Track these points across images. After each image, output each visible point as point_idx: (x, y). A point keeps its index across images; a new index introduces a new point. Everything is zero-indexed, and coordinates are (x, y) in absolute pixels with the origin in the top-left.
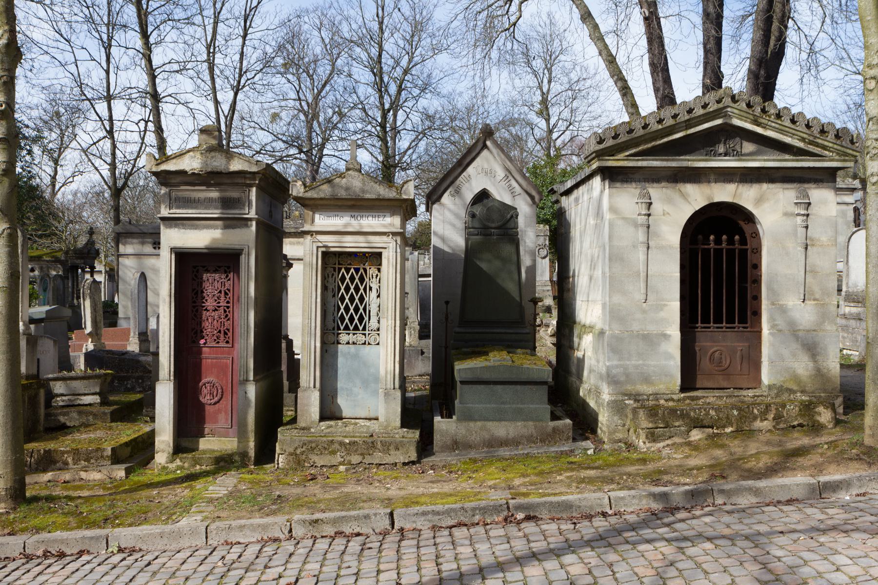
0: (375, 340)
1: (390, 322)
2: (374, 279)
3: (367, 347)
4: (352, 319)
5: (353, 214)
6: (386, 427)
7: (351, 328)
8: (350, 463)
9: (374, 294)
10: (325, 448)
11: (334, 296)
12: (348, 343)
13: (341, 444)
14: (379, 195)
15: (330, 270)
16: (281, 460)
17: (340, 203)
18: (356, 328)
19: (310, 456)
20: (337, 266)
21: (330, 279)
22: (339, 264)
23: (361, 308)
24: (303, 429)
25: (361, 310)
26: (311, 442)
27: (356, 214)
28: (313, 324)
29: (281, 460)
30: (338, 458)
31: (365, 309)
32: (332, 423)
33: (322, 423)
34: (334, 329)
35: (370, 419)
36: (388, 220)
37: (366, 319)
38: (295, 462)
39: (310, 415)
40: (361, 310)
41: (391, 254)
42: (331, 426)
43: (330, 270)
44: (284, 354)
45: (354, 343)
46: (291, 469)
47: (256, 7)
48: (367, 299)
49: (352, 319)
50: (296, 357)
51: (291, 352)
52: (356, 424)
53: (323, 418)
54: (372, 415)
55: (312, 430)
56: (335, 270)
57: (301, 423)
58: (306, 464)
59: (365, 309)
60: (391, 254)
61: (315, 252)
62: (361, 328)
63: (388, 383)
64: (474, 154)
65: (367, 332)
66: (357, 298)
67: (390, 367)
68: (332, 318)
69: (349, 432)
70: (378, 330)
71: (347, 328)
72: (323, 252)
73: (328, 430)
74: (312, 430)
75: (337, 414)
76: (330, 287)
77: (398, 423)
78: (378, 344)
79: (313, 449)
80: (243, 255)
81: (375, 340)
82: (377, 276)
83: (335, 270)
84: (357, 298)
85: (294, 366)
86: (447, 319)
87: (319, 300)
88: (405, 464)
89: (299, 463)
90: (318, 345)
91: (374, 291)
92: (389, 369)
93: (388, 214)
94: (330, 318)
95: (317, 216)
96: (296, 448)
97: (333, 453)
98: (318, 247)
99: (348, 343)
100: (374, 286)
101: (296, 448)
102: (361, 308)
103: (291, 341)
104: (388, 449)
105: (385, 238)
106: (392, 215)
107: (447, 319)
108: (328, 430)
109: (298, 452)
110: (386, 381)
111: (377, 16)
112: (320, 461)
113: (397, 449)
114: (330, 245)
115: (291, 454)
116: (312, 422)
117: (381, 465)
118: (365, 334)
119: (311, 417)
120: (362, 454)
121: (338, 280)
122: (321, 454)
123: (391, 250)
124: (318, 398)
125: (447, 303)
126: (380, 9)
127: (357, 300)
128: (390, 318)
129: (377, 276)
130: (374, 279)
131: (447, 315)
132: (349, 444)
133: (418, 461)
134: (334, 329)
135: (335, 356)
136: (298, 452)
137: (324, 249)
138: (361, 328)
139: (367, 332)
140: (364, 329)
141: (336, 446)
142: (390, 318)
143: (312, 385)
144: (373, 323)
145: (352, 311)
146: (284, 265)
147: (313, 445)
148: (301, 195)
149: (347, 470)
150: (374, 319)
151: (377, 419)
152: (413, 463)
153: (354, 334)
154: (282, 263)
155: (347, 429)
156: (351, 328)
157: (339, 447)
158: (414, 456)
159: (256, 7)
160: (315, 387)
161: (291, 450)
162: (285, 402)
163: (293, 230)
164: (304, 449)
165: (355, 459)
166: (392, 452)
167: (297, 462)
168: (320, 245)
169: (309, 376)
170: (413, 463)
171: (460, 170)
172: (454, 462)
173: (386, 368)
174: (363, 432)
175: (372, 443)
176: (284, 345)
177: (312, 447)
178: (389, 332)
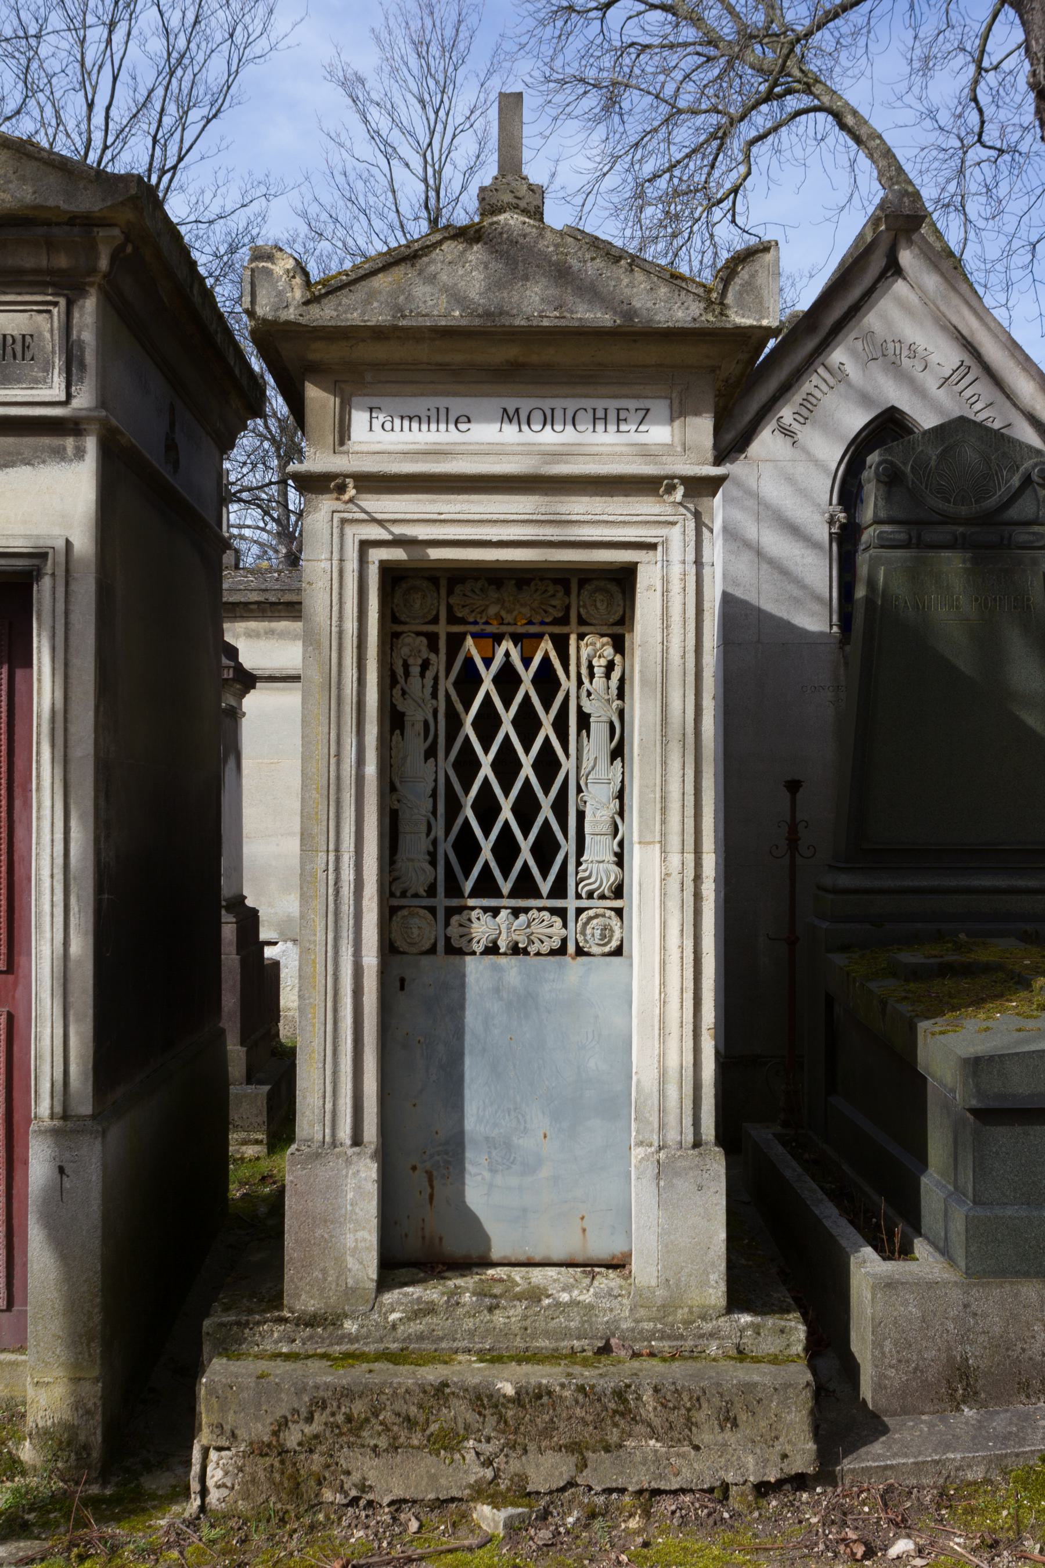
0: (606, 933)
1: (675, 859)
2: (599, 681)
3: (573, 967)
4: (506, 850)
5: (511, 404)
6: (666, 1309)
7: (506, 887)
8: (523, 1494)
9: (597, 744)
10: (410, 1422)
11: (431, 753)
12: (492, 950)
13: (483, 1400)
14: (630, 314)
15: (413, 646)
16: (217, 1471)
17: (458, 358)
18: (526, 887)
19: (347, 1458)
20: (442, 629)
21: (415, 681)
22: (452, 619)
23: (546, 802)
24: (311, 1321)
25: (546, 812)
26: (347, 1393)
27: (525, 405)
28: (348, 875)
29: (215, 1475)
30: (469, 1469)
31: (560, 807)
32: (431, 1293)
33: (389, 1297)
34: (432, 891)
35: (589, 1266)
36: (659, 433)
37: (568, 847)
38: (276, 1486)
39: (339, 1261)
40: (546, 812)
41: (676, 570)
42: (430, 1309)
43: (413, 646)
44: (230, 958)
45: (516, 950)
46: (262, 1516)
47: (174, 168)
48: (568, 765)
49: (506, 850)
50: (269, 952)
51: (250, 941)
52: (535, 1295)
53: (398, 1264)
54: (601, 1247)
55: (350, 1326)
56: (433, 647)
57: (303, 1295)
58: (328, 1495)
59: (560, 807)
60: (676, 570)
61: (352, 565)
62: (545, 887)
63: (672, 1119)
64: (856, 293)
65: (571, 904)
66: (527, 761)
67: (677, 1054)
68: (424, 844)
69: (506, 1333)
70: (618, 892)
71: (486, 886)
72: (387, 570)
73: (416, 1327)
74: (350, 1326)
75: (455, 1246)
76: (416, 715)
77: (716, 1293)
78: (618, 952)
79: (355, 1426)
80: (46, 582)
81: (606, 933)
82: (610, 667)
83: (433, 647)
84: (527, 761)
85: (277, 1067)
86: (793, 842)
87: (371, 769)
88: (763, 1489)
89: (296, 1491)
90: (371, 960)
91: (598, 730)
92: (672, 1061)
93: (660, 407)
94: (414, 845)
95: (359, 419)
96: (283, 1424)
97: (447, 1442)
98: (365, 545)
99: (492, 950)
100: (599, 711)
101: (283, 1424)
102: (546, 802)
103: (254, 913)
104: (690, 1423)
105: (646, 507)
106: (679, 412)
107: (793, 842)
108: (416, 1327)
109: (292, 1438)
110: (662, 1110)
111: (427, 207)
112: (389, 1479)
113: (729, 1420)
114: (422, 533)
115: (259, 1450)
116: (350, 1293)
117: (657, 1492)
118: (562, 913)
119: (342, 1270)
120: (575, 1448)
121: (447, 685)
122: (394, 1448)
123: (676, 552)
124: (372, 1189)
125: (793, 786)
126: (432, 194)
127: (527, 771)
128: (674, 841)
129: (610, 667)
130: (599, 681)
131: (793, 827)
132: (517, 1400)
133: (825, 1473)
134: (432, 891)
135: (450, 1002)
136: (292, 1438)
137: (398, 554)
138: (545, 887)
139: (571, 904)
140: (559, 890)
141: (460, 1411)
142: (674, 841)
143: (345, 1133)
144: (597, 865)
145: (506, 814)
146: (229, 674)
147: (359, 1408)
148: (291, 314)
149: (514, 1529)
150: (599, 851)
151: (618, 1265)
152: (800, 1482)
153: (516, 912)
154: (221, 668)
155: (499, 1319)
156: (506, 887)
157: (471, 1417)
158: (803, 1456)
159: (174, 168)
160: (357, 1140)
161: (262, 1431)
162: (234, 1116)
163: (254, 597)
164: (315, 1428)
165: (545, 1470)
166: (705, 1437)
167: (291, 1484)
168: (375, 533)
169: (334, 1077)
170: (800, 1482)
171: (810, 345)
172: (976, 1474)
173: (662, 1056)
174: (566, 1334)
175: (620, 1395)
176: (229, 931)
177: (351, 1419)
178: (673, 905)
